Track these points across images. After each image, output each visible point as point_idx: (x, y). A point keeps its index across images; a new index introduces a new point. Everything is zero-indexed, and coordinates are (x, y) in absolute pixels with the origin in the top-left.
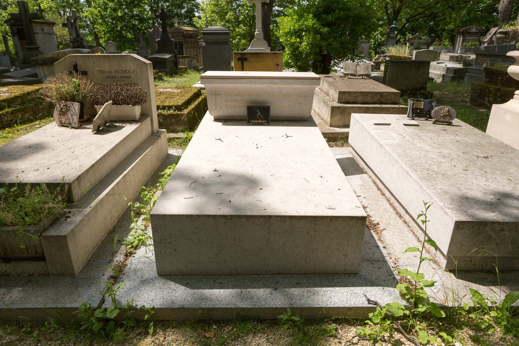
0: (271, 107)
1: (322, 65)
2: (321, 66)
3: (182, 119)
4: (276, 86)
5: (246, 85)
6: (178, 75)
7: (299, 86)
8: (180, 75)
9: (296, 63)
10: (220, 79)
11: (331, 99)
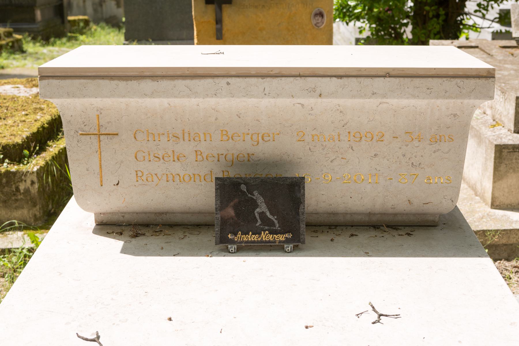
0: (308, 180)
1: (442, 12)
2: (438, 16)
3: (22, 187)
4: (325, 102)
5: (212, 102)
6: (64, 40)
7: (413, 102)
8: (70, 39)
9: (371, 9)
10: (103, 77)
11: (489, 118)
